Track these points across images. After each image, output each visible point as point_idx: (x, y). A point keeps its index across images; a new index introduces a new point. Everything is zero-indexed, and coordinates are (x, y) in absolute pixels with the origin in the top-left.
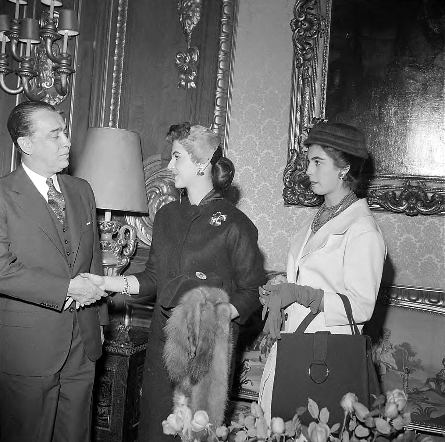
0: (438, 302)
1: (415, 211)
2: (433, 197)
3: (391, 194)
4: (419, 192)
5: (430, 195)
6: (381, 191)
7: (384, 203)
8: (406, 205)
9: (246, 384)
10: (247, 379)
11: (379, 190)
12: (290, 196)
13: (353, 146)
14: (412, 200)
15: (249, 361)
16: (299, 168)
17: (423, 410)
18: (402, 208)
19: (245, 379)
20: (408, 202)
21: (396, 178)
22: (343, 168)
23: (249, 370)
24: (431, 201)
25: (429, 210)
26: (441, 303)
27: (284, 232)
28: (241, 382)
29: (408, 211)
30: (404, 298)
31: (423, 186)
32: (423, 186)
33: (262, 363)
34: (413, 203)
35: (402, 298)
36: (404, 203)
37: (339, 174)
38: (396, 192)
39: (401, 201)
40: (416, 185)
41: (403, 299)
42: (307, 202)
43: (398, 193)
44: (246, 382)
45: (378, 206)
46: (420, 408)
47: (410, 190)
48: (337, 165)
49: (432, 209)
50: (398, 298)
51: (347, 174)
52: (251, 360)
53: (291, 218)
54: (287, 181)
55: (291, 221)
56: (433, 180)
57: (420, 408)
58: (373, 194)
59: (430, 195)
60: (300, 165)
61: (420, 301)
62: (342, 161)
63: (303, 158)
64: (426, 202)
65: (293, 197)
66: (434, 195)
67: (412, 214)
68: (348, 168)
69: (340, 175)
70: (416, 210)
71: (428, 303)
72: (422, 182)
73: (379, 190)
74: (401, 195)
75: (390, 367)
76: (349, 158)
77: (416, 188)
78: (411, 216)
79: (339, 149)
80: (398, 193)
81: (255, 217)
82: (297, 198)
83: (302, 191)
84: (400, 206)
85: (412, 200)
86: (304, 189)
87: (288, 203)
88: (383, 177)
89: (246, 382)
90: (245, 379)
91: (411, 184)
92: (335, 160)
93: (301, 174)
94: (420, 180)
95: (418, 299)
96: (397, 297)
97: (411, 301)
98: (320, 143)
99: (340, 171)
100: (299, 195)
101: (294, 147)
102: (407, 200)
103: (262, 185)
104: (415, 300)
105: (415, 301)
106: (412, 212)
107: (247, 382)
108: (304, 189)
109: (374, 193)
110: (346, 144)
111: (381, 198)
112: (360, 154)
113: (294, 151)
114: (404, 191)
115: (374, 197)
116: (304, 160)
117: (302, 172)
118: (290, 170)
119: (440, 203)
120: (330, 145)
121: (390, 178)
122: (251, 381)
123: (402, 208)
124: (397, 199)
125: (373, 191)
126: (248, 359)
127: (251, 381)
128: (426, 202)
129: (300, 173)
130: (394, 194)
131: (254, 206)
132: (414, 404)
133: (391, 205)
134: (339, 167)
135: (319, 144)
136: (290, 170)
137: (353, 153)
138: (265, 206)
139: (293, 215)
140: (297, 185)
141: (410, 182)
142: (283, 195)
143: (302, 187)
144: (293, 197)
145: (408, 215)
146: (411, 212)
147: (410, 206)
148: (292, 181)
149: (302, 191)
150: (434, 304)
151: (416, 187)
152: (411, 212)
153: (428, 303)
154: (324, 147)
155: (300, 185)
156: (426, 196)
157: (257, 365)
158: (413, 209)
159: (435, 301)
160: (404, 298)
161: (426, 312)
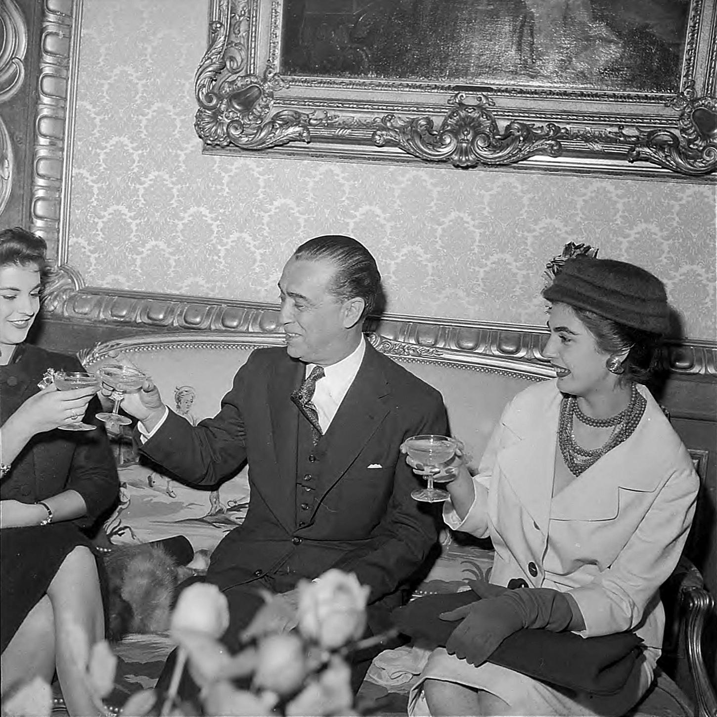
0: (517, 351)
1: (471, 157)
2: (508, 128)
3: (423, 122)
4: (481, 118)
5: (502, 124)
6: (404, 117)
7: (407, 141)
8: (452, 145)
9: (120, 535)
10: (121, 526)
11: (400, 116)
12: (211, 128)
13: (637, 310)
14: (466, 133)
15: (126, 487)
16: (231, 68)
17: (481, 573)
18: (445, 150)
19: (119, 525)
20: (456, 138)
21: (433, 89)
22: (615, 352)
23: (125, 506)
24: (505, 137)
25: (500, 154)
26: (522, 354)
27: (204, 210)
28: (108, 532)
29: (456, 158)
30: (449, 345)
31: (489, 105)
32: (489, 105)
33: (154, 490)
34: (468, 140)
35: (445, 345)
36: (448, 141)
37: (607, 362)
38: (433, 119)
39: (441, 135)
40: (475, 102)
41: (447, 347)
42: (247, 139)
43: (438, 121)
44: (120, 532)
45: (397, 150)
46: (475, 570)
47: (461, 113)
48: (604, 345)
49: (506, 152)
51: (622, 363)
52: (132, 485)
53: (219, 180)
54: (203, 93)
55: (219, 187)
56: (510, 92)
57: (475, 570)
58: (386, 125)
59: (502, 124)
60: (232, 59)
61: (480, 350)
62: (616, 339)
63: (240, 43)
64: (494, 138)
65: (216, 130)
66: (512, 123)
67: (465, 165)
68: (626, 353)
69: (609, 364)
70: (473, 156)
71: (497, 353)
72: (486, 97)
73: (400, 116)
74: (445, 124)
76: (629, 334)
77: (474, 109)
78: (463, 168)
79: (609, 316)
80: (438, 121)
81: (182, 214)
82: (225, 131)
83: (236, 115)
84: (440, 147)
85: (466, 133)
86: (240, 111)
87: (211, 145)
88: (408, 86)
89: (120, 532)
90: (119, 525)
91: (463, 102)
92: (600, 335)
93: (234, 81)
94: (484, 93)
95: (476, 346)
96: (436, 342)
97: (462, 349)
98: (572, 301)
99: (609, 357)
100: (229, 123)
101: (220, 18)
102: (455, 133)
103: (156, 109)
104: (472, 349)
105: (471, 350)
107: (122, 531)
108: (240, 111)
109: (390, 121)
110: (623, 306)
111: (402, 130)
112: (652, 325)
113: (218, 25)
114: (450, 117)
115: (388, 129)
116: (241, 50)
117: (238, 75)
118: (210, 69)
119: (523, 141)
120: (589, 307)
121: (422, 88)
122: (130, 529)
123: (445, 150)
124: (435, 133)
125: (387, 116)
126: (125, 483)
127: (130, 529)
128: (494, 138)
129: (234, 77)
130: (429, 122)
131: (178, 189)
132: (466, 562)
133: (422, 143)
134: (607, 350)
135: (569, 304)
136: (210, 69)
137: (635, 324)
138: (125, 119)
139: (223, 174)
140: (224, 102)
141: (462, 96)
142: (195, 126)
143: (237, 107)
144: (216, 130)
145: (457, 167)
146: (464, 159)
147: (462, 148)
148: (215, 94)
149: (236, 115)
150: (509, 356)
151: (474, 107)
152: (464, 159)
153: (497, 353)
154: (578, 310)
155: (231, 104)
156: (494, 126)
157: (143, 494)
158: (466, 152)
159: (511, 349)
160: (449, 345)
161: (490, 370)
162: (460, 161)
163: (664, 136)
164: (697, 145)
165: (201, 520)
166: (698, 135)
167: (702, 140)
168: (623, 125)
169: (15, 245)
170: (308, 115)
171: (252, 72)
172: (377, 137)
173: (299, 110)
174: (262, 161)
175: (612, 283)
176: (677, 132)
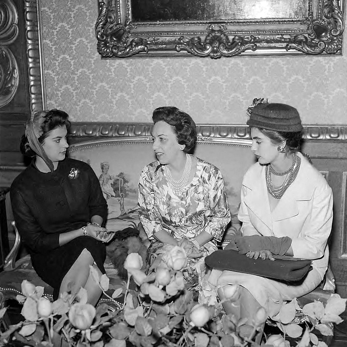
1: (219, 54)
5: (231, 38)
50: (211, 136)
59: (231, 38)
65: (107, 50)
68: (284, 143)
75: (109, 195)
106: (216, 56)
124: (202, 44)
130: (199, 39)
139: (111, 68)
158: (216, 52)
162: (214, 56)
163: (301, 38)
164: (315, 41)
165: (118, 218)
166: (315, 36)
167: (317, 38)
168: (283, 34)
169: (58, 118)
170: (146, 39)
171: (120, 22)
172: (177, 48)
173: (142, 38)
174: (128, 60)
175: (272, 114)
176: (307, 35)
